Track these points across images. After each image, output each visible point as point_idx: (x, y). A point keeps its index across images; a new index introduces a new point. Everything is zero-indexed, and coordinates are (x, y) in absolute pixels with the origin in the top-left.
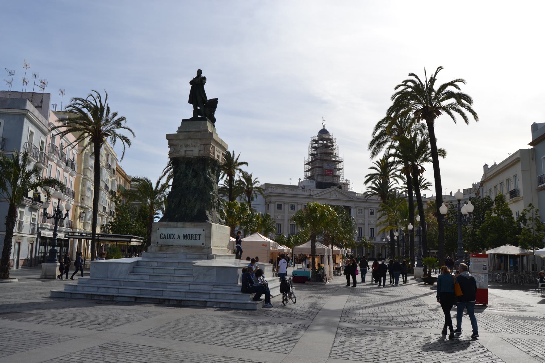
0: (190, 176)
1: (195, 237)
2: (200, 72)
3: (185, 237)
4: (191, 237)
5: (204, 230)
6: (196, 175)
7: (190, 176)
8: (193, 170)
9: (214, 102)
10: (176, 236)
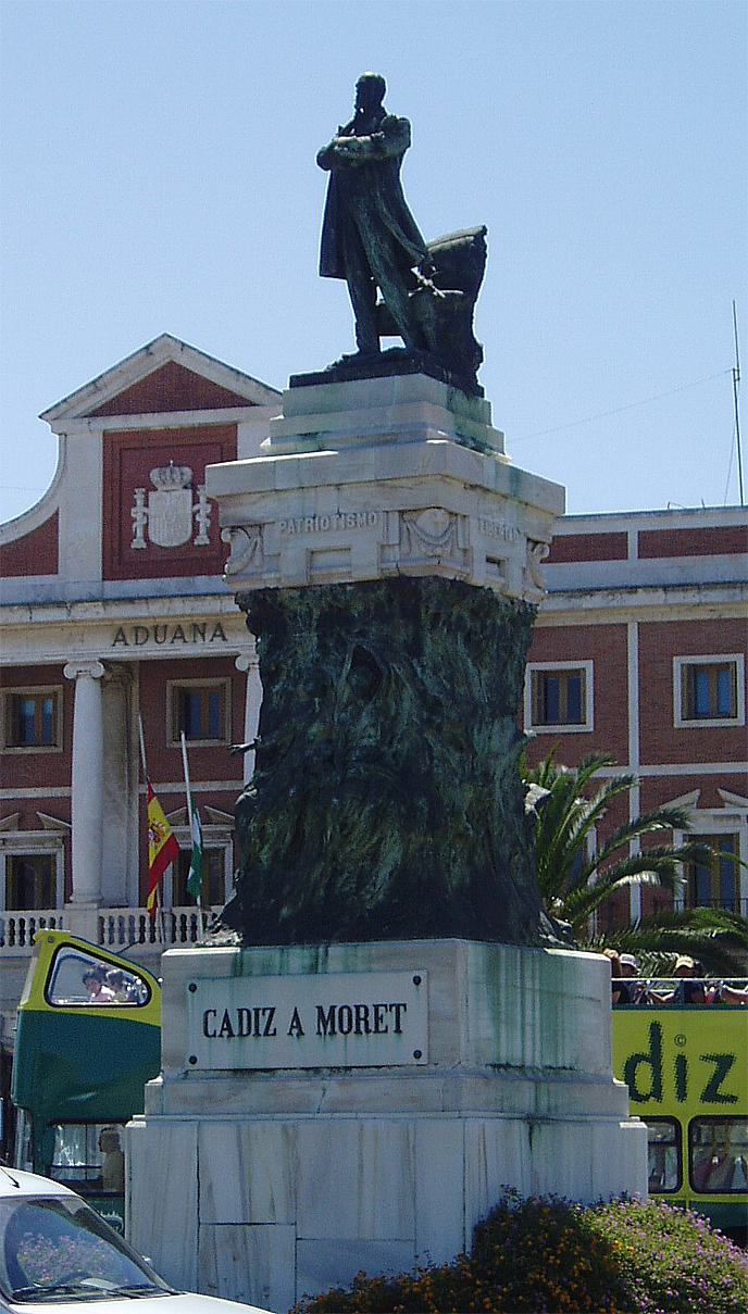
0: (344, 691)
1: (378, 1019)
2: (371, 91)
3: (328, 1020)
4: (360, 1020)
5: (417, 981)
6: (372, 679)
7: (344, 691)
8: (361, 659)
9: (465, 262)
10: (282, 1022)
